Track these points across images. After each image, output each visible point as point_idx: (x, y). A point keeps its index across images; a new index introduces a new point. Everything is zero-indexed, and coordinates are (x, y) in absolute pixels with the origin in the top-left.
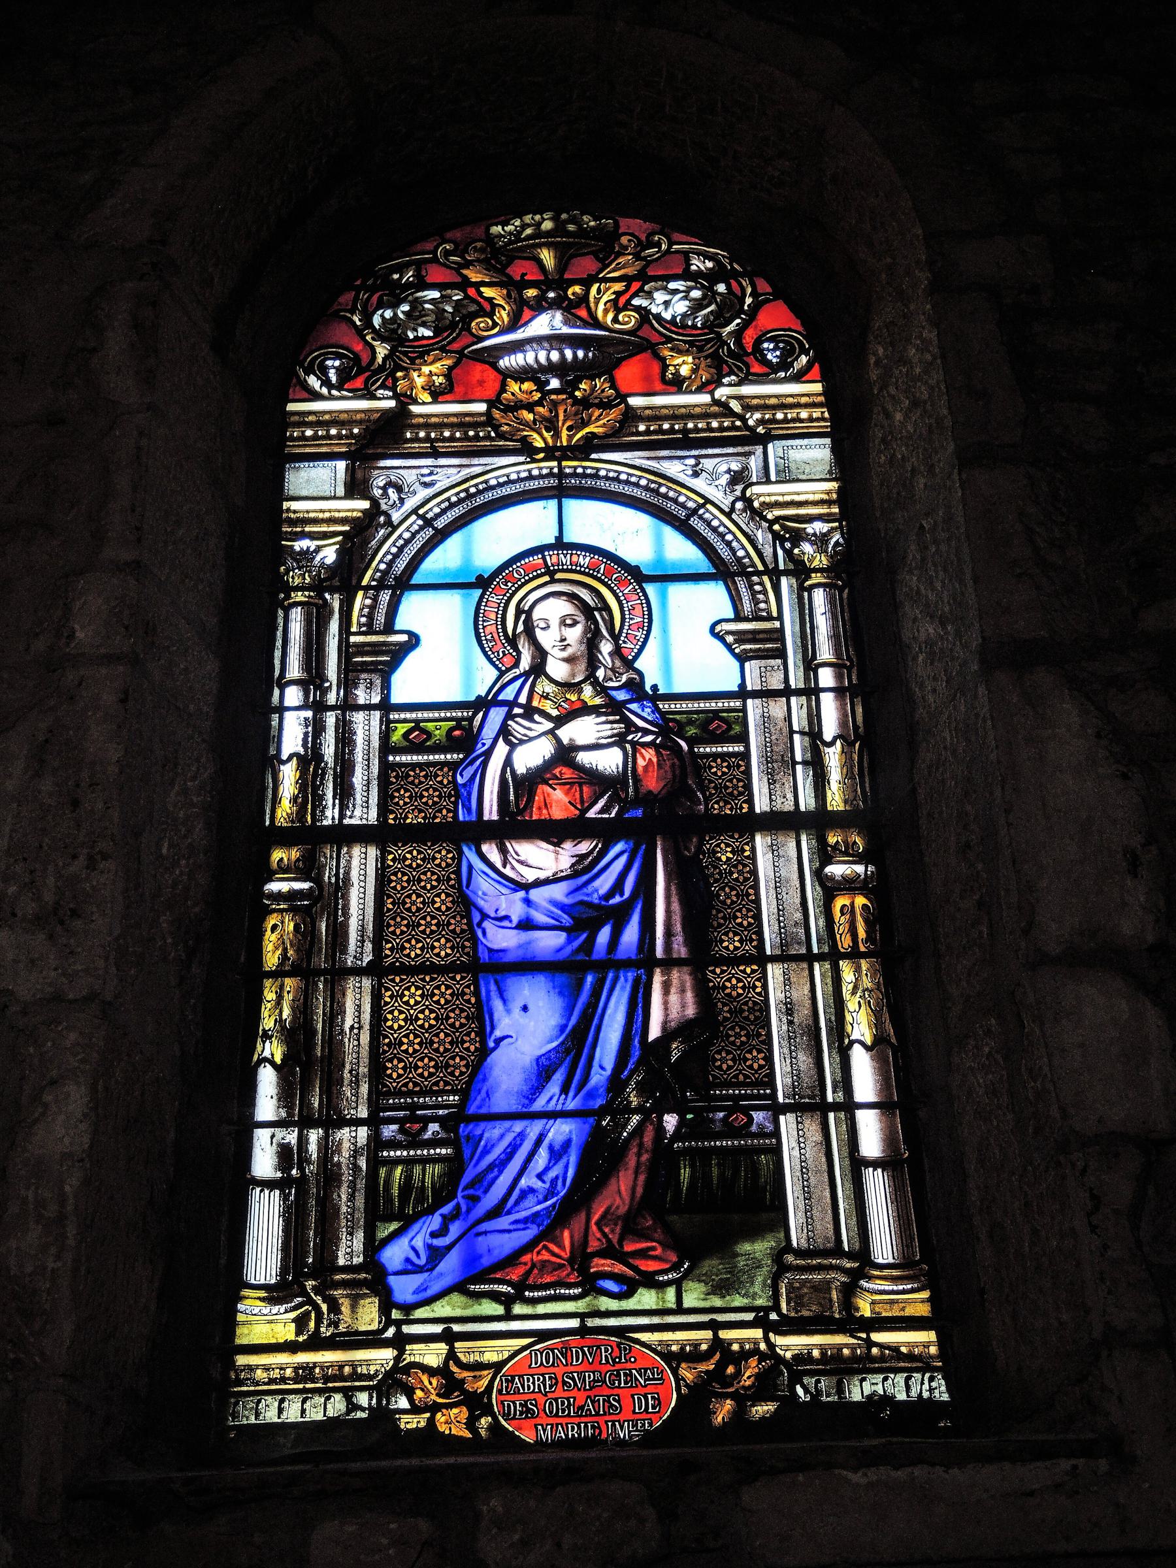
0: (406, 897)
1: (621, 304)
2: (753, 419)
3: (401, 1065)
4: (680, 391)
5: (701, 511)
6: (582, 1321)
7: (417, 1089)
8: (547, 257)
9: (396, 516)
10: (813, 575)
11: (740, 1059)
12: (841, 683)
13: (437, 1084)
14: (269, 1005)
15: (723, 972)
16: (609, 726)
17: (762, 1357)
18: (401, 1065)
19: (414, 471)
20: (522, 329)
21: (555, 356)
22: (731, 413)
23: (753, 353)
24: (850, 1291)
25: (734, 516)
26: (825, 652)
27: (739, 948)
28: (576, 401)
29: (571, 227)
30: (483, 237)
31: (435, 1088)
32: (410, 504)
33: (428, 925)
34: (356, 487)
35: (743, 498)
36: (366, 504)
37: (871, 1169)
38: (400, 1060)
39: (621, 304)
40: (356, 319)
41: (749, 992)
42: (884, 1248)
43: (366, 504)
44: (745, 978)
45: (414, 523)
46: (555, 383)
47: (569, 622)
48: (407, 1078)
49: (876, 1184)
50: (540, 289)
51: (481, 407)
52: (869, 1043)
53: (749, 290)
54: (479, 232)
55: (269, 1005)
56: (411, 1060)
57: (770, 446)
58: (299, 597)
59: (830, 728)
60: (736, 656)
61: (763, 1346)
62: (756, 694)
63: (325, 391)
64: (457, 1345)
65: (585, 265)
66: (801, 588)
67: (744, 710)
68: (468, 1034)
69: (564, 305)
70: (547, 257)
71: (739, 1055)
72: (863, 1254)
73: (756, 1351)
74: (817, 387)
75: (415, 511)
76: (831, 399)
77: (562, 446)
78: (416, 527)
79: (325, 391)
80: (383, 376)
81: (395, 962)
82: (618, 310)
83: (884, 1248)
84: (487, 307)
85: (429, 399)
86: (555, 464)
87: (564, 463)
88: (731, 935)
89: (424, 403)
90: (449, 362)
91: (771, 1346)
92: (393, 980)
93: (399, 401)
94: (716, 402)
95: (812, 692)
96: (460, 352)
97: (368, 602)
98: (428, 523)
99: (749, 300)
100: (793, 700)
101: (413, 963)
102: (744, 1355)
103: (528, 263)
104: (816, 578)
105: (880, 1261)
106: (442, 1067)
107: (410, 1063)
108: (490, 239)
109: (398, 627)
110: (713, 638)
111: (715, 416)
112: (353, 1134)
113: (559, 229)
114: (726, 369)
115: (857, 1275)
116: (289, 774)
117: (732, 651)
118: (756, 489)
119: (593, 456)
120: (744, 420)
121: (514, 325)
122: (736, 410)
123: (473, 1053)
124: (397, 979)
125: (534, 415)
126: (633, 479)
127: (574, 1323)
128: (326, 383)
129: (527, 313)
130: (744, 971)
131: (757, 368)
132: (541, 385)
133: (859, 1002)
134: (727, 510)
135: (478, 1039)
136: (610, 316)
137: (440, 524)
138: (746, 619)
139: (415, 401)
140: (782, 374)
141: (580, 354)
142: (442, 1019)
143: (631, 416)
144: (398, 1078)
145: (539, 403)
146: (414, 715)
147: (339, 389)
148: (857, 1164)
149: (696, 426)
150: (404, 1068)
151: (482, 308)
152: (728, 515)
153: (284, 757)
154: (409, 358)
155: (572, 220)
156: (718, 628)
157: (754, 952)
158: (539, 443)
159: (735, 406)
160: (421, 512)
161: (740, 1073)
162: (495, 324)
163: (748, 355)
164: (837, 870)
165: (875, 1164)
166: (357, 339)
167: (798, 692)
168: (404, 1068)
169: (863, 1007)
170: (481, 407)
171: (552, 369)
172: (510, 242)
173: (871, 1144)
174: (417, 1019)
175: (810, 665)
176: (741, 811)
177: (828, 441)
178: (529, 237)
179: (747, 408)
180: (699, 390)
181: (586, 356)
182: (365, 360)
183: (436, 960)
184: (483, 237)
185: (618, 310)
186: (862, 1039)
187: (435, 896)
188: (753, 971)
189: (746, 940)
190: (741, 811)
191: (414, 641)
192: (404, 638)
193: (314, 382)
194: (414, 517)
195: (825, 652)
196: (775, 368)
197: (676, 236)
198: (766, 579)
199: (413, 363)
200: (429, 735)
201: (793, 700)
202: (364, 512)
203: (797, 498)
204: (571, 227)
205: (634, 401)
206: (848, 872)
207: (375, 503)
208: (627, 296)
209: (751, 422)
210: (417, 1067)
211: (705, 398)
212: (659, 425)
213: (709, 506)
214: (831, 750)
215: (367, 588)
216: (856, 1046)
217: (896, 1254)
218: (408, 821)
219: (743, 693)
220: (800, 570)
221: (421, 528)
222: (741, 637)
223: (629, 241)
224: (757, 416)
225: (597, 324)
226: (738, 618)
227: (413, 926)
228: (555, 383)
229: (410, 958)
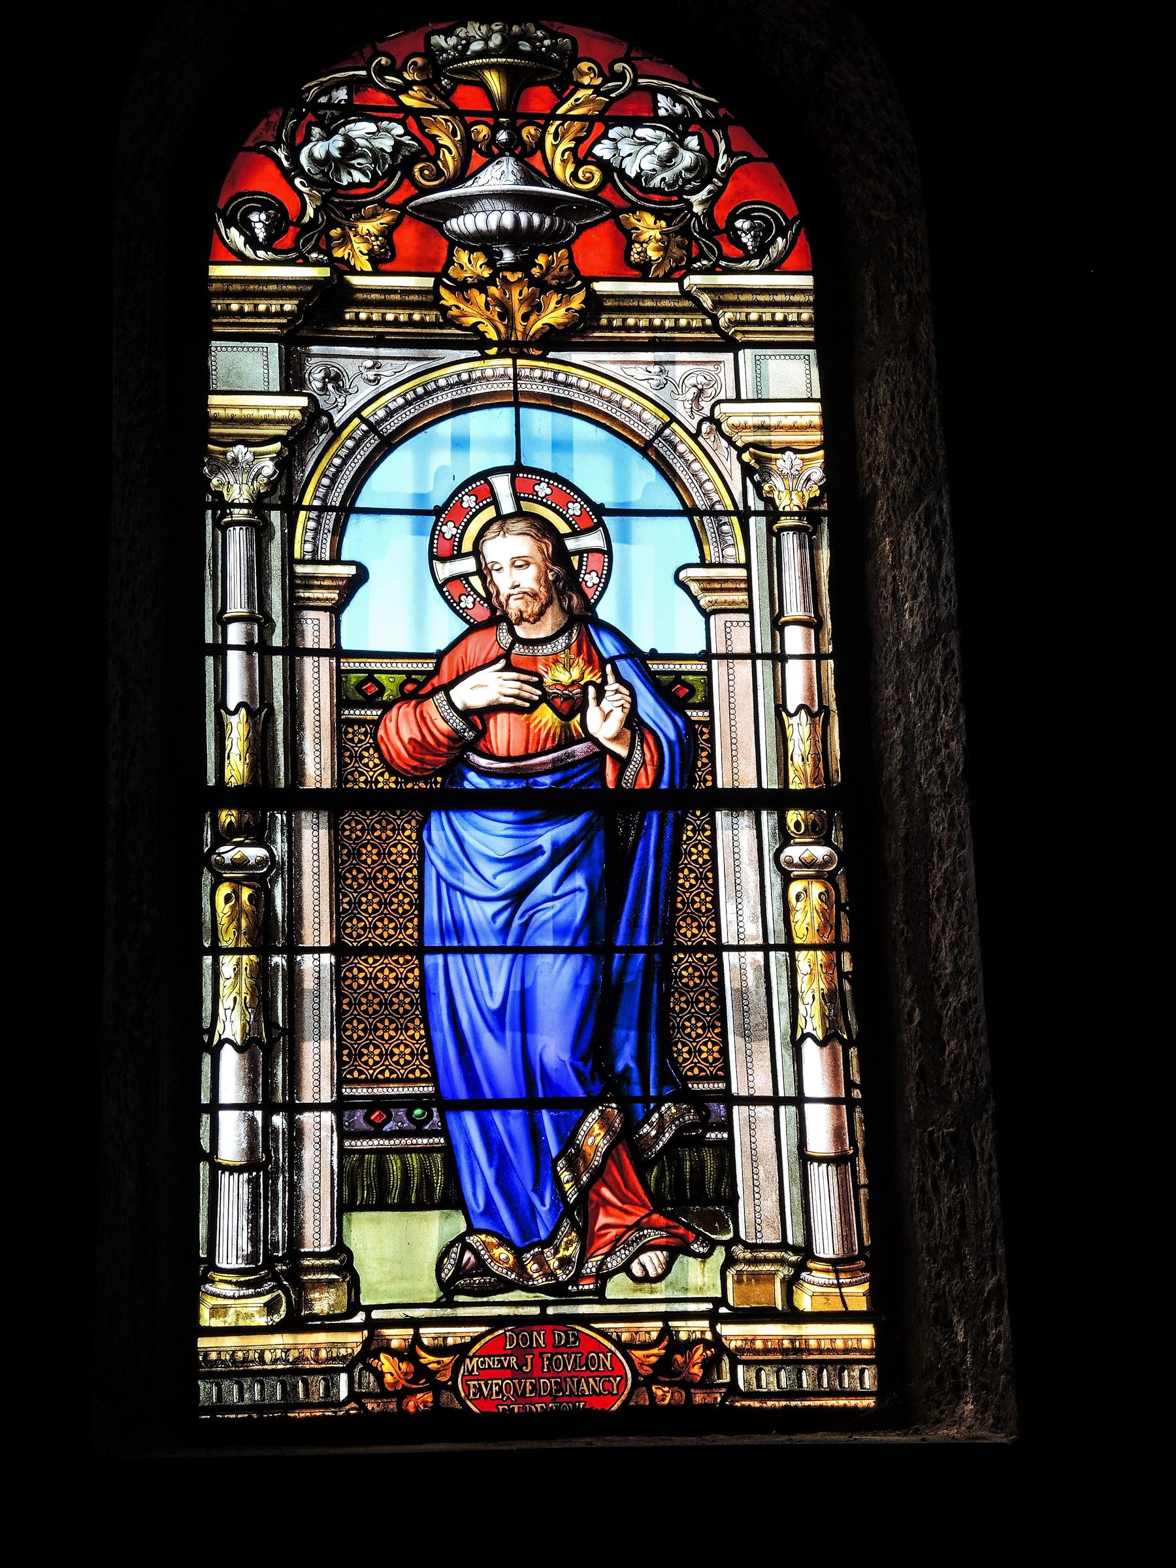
0: (377, 872)
1: (581, 155)
2: (726, 317)
3: (377, 1051)
4: (645, 278)
5: (667, 432)
6: (543, 1310)
7: (394, 1076)
8: (494, 82)
9: (338, 418)
10: (783, 518)
11: (695, 1052)
12: (809, 649)
13: (413, 1071)
14: (229, 983)
15: (375, 961)
16: (518, 684)
17: (707, 1344)
18: (377, 1051)
19: (358, 362)
20: (471, 182)
21: (508, 221)
22: (699, 308)
23: (727, 230)
24: (790, 1284)
25: (700, 439)
26: (794, 607)
27: (697, 935)
28: (533, 282)
29: (525, 46)
30: (423, 50)
31: (411, 1076)
32: (353, 403)
33: (401, 903)
34: (292, 382)
35: (711, 419)
36: (303, 402)
37: (227, 1174)
38: (376, 1047)
39: (581, 155)
40: (281, 154)
41: (706, 982)
42: (827, 1244)
43: (303, 402)
44: (702, 967)
45: (358, 427)
46: (508, 256)
47: (518, 563)
48: (383, 1065)
49: (822, 1180)
50: (538, 125)
51: (429, 282)
52: (239, 1042)
53: (722, 146)
54: (415, 40)
55: (229, 983)
56: (387, 1046)
57: (741, 353)
58: (239, 514)
59: (795, 696)
60: (702, 611)
61: (709, 1336)
62: (720, 657)
63: (249, 252)
64: (422, 1330)
65: (538, 98)
66: (770, 532)
67: (709, 673)
68: (412, 1021)
69: (517, 152)
70: (494, 82)
71: (695, 1048)
72: (806, 1251)
73: (702, 1341)
74: (807, 281)
75: (357, 414)
76: (822, 298)
77: (517, 341)
78: (358, 434)
79: (249, 252)
80: (315, 233)
81: (368, 942)
82: (579, 164)
83: (827, 1244)
84: (432, 151)
85: (368, 267)
86: (509, 361)
87: (519, 362)
88: (689, 920)
89: (363, 273)
90: (387, 219)
91: (717, 1337)
92: (366, 961)
93: (334, 270)
94: (685, 294)
95: (779, 658)
96: (402, 207)
97: (312, 524)
98: (373, 428)
99: (722, 160)
100: (759, 662)
101: (386, 944)
102: (690, 1345)
103: (473, 89)
104: (785, 522)
105: (822, 1255)
106: (417, 1054)
107: (386, 1050)
108: (430, 53)
109: (344, 557)
110: (677, 587)
111: (684, 311)
112: (318, 1120)
113: (509, 47)
114: (695, 251)
115: (800, 1267)
116: (238, 728)
117: (695, 601)
118: (725, 407)
119: (551, 355)
120: (715, 319)
121: (461, 177)
122: (705, 305)
123: (679, 1041)
124: (371, 960)
125: (487, 296)
126: (596, 388)
127: (535, 1311)
128: (252, 241)
129: (477, 160)
130: (397, 962)
131: (729, 249)
132: (492, 260)
133: (235, 998)
134: (694, 431)
135: (422, 1026)
136: (570, 168)
137: (389, 427)
138: (712, 565)
139: (354, 272)
140: (756, 262)
141: (536, 219)
142: (692, 1002)
143: (595, 302)
144: (374, 1065)
145: (491, 281)
146: (404, 667)
147: (266, 248)
148: (805, 1158)
149: (242, 309)
150: (380, 1055)
151: (423, 149)
152: (695, 437)
153: (232, 706)
154: (344, 212)
155: (524, 36)
156: (682, 575)
157: (713, 939)
158: (492, 335)
159: (707, 301)
160: (365, 413)
161: (696, 1066)
162: (440, 173)
163: (719, 232)
164: (794, 853)
165: (821, 1160)
166: (284, 183)
167: (764, 656)
168: (380, 1055)
169: (238, 1007)
170: (429, 282)
171: (502, 235)
172: (455, 60)
173: (820, 1141)
174: (392, 1003)
175: (778, 625)
176: (376, 786)
177: (812, 352)
178: (478, 55)
179: (718, 304)
180: (666, 278)
181: (542, 222)
182: (293, 215)
183: (378, 940)
184: (423, 50)
185: (579, 164)
186: (814, 1033)
187: (406, 871)
188: (710, 960)
189: (704, 927)
190: (376, 786)
191: (362, 575)
192: (352, 570)
193: (236, 238)
194: (356, 421)
195: (794, 607)
196: (749, 257)
197: (645, 65)
198: (735, 519)
199: (348, 218)
200: (382, 689)
201: (759, 662)
202: (303, 410)
203: (254, 413)
204: (525, 46)
205: (600, 287)
206: (806, 855)
207: (312, 399)
208: (588, 142)
209: (722, 322)
210: (392, 1054)
211: (672, 288)
212: (650, 319)
213: (674, 426)
214: (234, 719)
215: (310, 508)
216: (809, 1041)
217: (836, 1249)
218: (380, 786)
219: (706, 656)
220: (772, 513)
221: (366, 434)
222: (709, 585)
223: (590, 68)
224: (729, 315)
225: (554, 181)
226: (703, 564)
227: (386, 904)
228: (508, 256)
229: (383, 938)
